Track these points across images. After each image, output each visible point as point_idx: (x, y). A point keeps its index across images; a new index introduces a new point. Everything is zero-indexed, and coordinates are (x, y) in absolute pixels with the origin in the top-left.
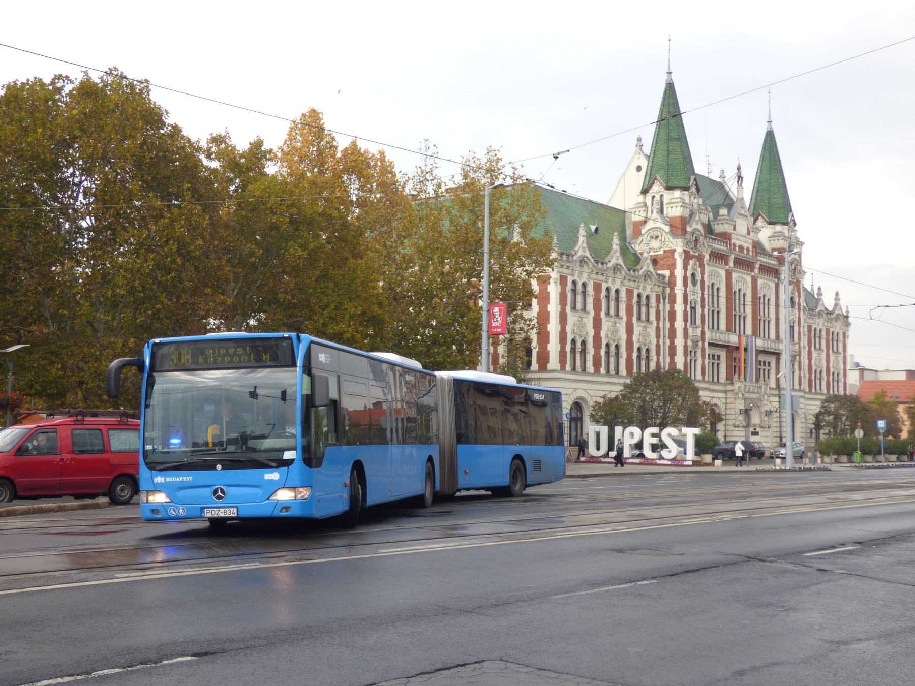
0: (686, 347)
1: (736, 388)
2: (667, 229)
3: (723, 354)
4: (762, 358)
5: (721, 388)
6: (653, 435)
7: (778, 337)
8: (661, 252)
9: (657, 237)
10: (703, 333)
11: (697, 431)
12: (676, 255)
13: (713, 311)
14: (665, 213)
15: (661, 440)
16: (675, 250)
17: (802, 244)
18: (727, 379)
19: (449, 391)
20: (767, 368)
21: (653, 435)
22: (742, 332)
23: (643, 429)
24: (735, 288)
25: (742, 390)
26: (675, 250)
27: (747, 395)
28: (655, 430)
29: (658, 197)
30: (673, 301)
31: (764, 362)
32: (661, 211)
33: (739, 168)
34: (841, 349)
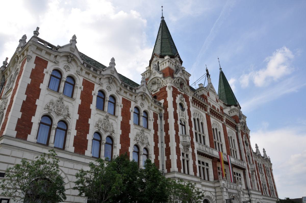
0: (178, 149)
1: (222, 185)
2: (161, 76)
3: (210, 162)
4: (235, 170)
5: (211, 185)
7: (242, 159)
8: (159, 90)
10: (192, 143)
12: (167, 89)
17: (246, 117)
18: (215, 179)
20: (239, 177)
22: (221, 151)
24: (229, 135)
25: (226, 186)
26: (166, 86)
27: (229, 190)
30: (166, 117)
31: (237, 174)
33: (207, 71)
34: (271, 175)
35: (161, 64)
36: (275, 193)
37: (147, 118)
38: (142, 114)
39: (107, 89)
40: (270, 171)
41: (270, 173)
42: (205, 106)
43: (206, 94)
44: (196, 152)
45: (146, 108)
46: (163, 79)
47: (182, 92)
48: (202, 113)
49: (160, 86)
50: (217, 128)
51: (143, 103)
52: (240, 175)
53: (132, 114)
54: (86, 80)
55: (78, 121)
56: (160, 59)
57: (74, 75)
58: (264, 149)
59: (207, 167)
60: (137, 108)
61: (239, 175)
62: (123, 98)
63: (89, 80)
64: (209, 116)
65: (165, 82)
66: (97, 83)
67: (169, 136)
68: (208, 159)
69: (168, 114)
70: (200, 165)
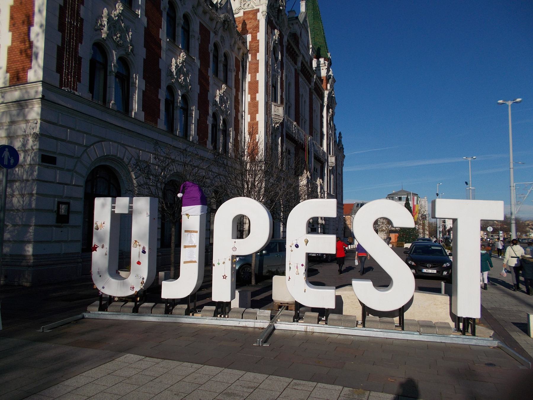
16: (258, 10)
26: (258, 10)
37: (187, 31)
44: (284, 134)
49: (246, 6)
67: (258, 102)
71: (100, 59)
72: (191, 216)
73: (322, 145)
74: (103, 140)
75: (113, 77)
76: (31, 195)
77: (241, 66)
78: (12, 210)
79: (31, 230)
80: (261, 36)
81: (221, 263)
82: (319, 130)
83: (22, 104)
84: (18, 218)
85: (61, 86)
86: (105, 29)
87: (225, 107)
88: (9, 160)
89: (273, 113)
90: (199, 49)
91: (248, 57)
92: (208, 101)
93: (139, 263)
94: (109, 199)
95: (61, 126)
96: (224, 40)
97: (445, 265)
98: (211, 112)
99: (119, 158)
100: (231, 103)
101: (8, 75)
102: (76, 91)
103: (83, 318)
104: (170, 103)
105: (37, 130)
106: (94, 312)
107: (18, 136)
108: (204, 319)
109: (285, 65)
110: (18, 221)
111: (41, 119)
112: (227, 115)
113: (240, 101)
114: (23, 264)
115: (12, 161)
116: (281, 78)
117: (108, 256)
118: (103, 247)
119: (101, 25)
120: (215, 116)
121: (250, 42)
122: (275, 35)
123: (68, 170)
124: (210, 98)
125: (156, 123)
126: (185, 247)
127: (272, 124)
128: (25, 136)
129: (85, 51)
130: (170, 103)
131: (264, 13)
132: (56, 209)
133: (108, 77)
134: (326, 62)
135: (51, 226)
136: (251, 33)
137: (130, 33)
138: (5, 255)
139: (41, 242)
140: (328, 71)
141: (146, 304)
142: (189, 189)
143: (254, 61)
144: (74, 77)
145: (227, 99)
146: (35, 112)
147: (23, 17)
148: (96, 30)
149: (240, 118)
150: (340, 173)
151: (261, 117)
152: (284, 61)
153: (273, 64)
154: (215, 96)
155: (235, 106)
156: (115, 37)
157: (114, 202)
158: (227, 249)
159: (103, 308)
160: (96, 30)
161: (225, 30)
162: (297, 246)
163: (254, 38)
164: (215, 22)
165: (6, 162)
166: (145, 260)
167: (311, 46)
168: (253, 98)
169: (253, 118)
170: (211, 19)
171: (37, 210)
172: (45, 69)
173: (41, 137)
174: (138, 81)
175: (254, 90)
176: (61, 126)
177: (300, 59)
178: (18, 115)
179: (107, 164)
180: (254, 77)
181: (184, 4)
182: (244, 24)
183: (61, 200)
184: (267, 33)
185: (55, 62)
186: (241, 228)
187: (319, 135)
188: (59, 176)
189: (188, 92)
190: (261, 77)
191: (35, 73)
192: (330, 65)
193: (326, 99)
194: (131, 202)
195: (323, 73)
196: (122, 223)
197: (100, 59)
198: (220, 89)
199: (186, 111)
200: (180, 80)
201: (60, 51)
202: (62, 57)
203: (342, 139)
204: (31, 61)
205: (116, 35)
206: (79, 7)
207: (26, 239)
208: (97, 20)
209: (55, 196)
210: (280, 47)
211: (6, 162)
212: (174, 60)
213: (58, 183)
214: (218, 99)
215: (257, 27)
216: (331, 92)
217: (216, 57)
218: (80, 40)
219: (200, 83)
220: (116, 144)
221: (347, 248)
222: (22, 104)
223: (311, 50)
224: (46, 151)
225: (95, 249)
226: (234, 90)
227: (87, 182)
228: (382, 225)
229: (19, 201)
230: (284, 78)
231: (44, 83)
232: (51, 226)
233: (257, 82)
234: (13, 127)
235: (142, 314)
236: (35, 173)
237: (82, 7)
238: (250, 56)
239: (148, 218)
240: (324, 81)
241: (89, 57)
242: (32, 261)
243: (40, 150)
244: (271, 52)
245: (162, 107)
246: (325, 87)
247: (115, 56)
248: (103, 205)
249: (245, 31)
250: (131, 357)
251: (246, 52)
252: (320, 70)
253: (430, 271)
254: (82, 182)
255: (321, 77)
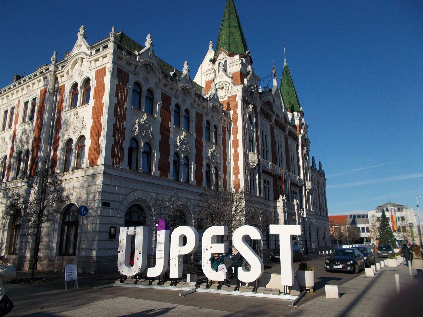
2: (230, 80)
6: (219, 239)
9: (223, 88)
11: (296, 229)
13: (263, 150)
14: (228, 71)
15: (230, 248)
16: (236, 95)
19: (65, 207)
21: (219, 239)
23: (200, 229)
24: (276, 139)
26: (236, 95)
28: (219, 230)
29: (223, 62)
31: (294, 192)
32: (225, 70)
35: (230, 65)
36: (325, 211)
37: (187, 118)
38: (144, 93)
39: (143, 80)
40: (323, 187)
41: (323, 189)
42: (271, 115)
43: (271, 100)
44: (261, 171)
45: (151, 85)
46: (232, 85)
47: (251, 101)
48: (267, 124)
49: (229, 93)
50: (264, 130)
51: (147, 78)
52: (268, 182)
53: (204, 129)
54: (164, 94)
55: (160, 142)
56: (228, 57)
57: (154, 88)
58: (320, 163)
59: (268, 186)
60: (137, 84)
61: (267, 183)
62: (196, 112)
63: (167, 92)
64: (273, 128)
65: (236, 90)
66: (131, 73)
67: (238, 153)
68: (270, 176)
69: (238, 128)
70: (265, 185)
71: (135, 146)
72: (161, 235)
73: (299, 175)
74: (135, 190)
75: (141, 155)
76: (97, 224)
77: (227, 130)
78: (88, 232)
79: (96, 243)
80: (239, 111)
81: (174, 258)
82: (296, 164)
83: (93, 176)
84: (90, 237)
85: (113, 165)
86: (137, 130)
87: (216, 159)
88: (84, 212)
89: (250, 159)
90: (196, 127)
91: (231, 124)
92: (203, 158)
93: (138, 259)
94: (126, 228)
95: (113, 186)
96: (213, 118)
97: (349, 263)
98: (205, 164)
99: (144, 199)
100: (220, 156)
101: (88, 161)
102: (121, 166)
103: (113, 286)
104: (176, 163)
105: (100, 190)
106: (118, 283)
107: (91, 193)
108: (167, 287)
109: (259, 125)
110: (90, 238)
111: (103, 184)
112: (217, 164)
113: (227, 154)
114: (91, 261)
115: (85, 213)
116: (257, 135)
117: (124, 256)
118: (123, 251)
119: (135, 128)
120: (208, 166)
121: (232, 115)
122: (249, 108)
123: (116, 209)
124: (204, 155)
125: (167, 176)
126: (158, 250)
127: (249, 166)
128: (95, 192)
129: (126, 144)
130: (176, 163)
131: (240, 97)
132: (109, 231)
133: (139, 155)
134: (299, 114)
135: (106, 240)
136: (233, 109)
137: (151, 129)
138: (83, 257)
139: (101, 249)
140: (301, 120)
141: (141, 280)
142: (160, 222)
143: (235, 127)
144: (120, 158)
145: (217, 154)
146: (100, 180)
147: (96, 132)
148: (132, 132)
149: (227, 164)
150: (323, 192)
151: (241, 163)
152: (259, 123)
153: (249, 127)
154: (208, 153)
155: (223, 157)
156: (142, 133)
157: (128, 229)
158: (177, 251)
159: (122, 282)
160: (132, 132)
161: (213, 112)
162: (207, 250)
163: (235, 113)
164: (206, 109)
165: (82, 214)
166: (140, 257)
167: (283, 107)
168: (236, 151)
169: (236, 164)
170: (204, 108)
171: (99, 232)
172: (106, 158)
173: (102, 193)
174: (156, 154)
175: (236, 145)
176: (113, 186)
177: (274, 117)
178: (92, 182)
179: (138, 203)
180: (235, 137)
181: (185, 103)
182: (228, 104)
183: (112, 226)
184: (243, 108)
185: (110, 153)
186: (184, 240)
187: (296, 167)
188: (111, 213)
189: (188, 154)
190: (240, 137)
191: (101, 160)
192: (303, 115)
193: (300, 141)
194: (135, 229)
195: (297, 122)
196: (132, 239)
197: (135, 146)
198: (211, 148)
199: (188, 165)
200: (182, 148)
201: (113, 147)
202: (114, 150)
203: (322, 167)
204: (99, 154)
205: (143, 132)
206: (123, 122)
207: (93, 248)
208: (133, 126)
209: (109, 224)
210: (254, 114)
211: (82, 214)
212: (178, 138)
213: (111, 217)
214: (209, 155)
215: (236, 106)
216: (304, 135)
217: (208, 129)
218: (123, 138)
219: (197, 147)
220: (142, 192)
221: (331, 252)
222: (93, 176)
223: (284, 109)
224: (105, 200)
225: (119, 252)
226: (222, 147)
227: (126, 215)
228: (247, 239)
229: (91, 227)
230: (259, 134)
231: (105, 165)
232: (106, 240)
233: (238, 140)
234: (90, 188)
235: (139, 285)
236: (99, 212)
237: (125, 122)
238: (232, 123)
239: (142, 237)
240: (298, 128)
241: (128, 147)
242: (96, 260)
243: (102, 200)
244: (248, 119)
245: (171, 166)
246: (299, 132)
247: (142, 143)
248: (123, 231)
249: (229, 108)
250: (124, 297)
251: (229, 121)
252: (294, 120)
253: (338, 267)
254: (123, 215)
255: (295, 125)
